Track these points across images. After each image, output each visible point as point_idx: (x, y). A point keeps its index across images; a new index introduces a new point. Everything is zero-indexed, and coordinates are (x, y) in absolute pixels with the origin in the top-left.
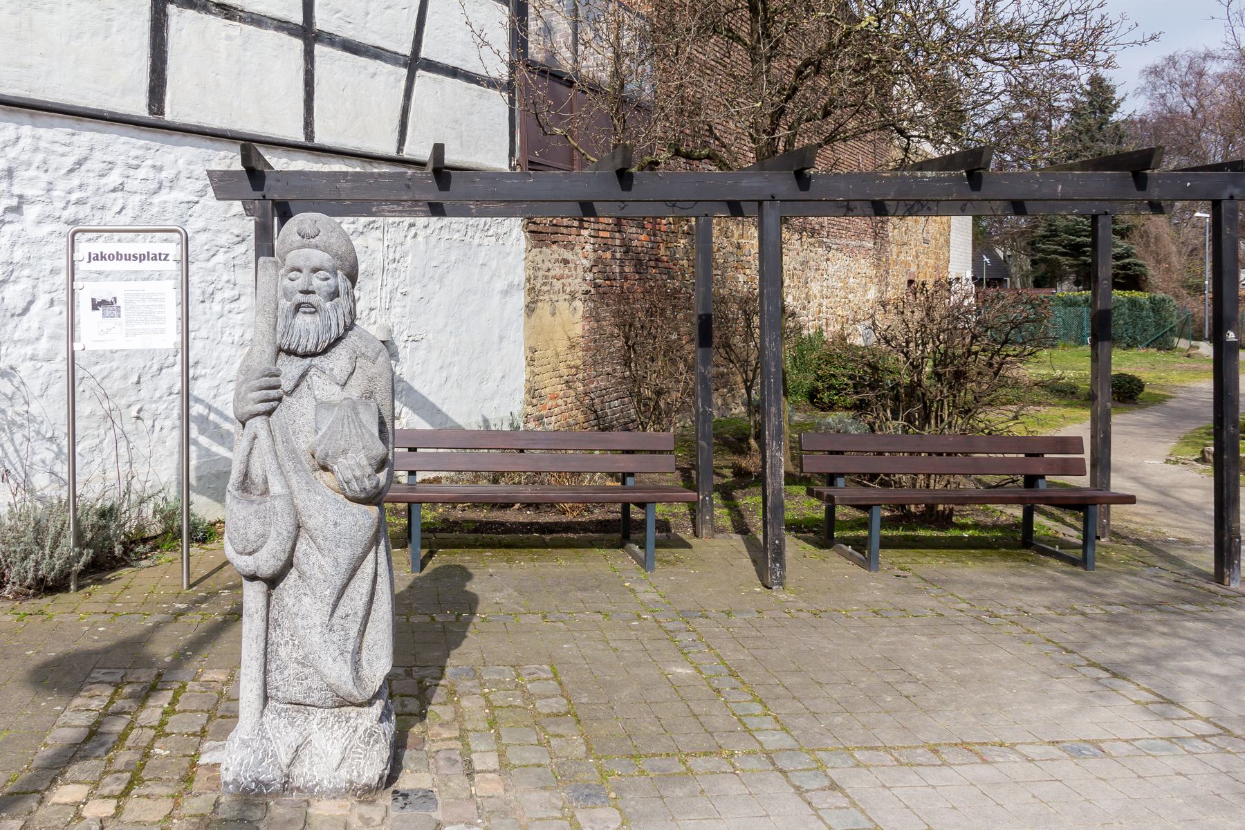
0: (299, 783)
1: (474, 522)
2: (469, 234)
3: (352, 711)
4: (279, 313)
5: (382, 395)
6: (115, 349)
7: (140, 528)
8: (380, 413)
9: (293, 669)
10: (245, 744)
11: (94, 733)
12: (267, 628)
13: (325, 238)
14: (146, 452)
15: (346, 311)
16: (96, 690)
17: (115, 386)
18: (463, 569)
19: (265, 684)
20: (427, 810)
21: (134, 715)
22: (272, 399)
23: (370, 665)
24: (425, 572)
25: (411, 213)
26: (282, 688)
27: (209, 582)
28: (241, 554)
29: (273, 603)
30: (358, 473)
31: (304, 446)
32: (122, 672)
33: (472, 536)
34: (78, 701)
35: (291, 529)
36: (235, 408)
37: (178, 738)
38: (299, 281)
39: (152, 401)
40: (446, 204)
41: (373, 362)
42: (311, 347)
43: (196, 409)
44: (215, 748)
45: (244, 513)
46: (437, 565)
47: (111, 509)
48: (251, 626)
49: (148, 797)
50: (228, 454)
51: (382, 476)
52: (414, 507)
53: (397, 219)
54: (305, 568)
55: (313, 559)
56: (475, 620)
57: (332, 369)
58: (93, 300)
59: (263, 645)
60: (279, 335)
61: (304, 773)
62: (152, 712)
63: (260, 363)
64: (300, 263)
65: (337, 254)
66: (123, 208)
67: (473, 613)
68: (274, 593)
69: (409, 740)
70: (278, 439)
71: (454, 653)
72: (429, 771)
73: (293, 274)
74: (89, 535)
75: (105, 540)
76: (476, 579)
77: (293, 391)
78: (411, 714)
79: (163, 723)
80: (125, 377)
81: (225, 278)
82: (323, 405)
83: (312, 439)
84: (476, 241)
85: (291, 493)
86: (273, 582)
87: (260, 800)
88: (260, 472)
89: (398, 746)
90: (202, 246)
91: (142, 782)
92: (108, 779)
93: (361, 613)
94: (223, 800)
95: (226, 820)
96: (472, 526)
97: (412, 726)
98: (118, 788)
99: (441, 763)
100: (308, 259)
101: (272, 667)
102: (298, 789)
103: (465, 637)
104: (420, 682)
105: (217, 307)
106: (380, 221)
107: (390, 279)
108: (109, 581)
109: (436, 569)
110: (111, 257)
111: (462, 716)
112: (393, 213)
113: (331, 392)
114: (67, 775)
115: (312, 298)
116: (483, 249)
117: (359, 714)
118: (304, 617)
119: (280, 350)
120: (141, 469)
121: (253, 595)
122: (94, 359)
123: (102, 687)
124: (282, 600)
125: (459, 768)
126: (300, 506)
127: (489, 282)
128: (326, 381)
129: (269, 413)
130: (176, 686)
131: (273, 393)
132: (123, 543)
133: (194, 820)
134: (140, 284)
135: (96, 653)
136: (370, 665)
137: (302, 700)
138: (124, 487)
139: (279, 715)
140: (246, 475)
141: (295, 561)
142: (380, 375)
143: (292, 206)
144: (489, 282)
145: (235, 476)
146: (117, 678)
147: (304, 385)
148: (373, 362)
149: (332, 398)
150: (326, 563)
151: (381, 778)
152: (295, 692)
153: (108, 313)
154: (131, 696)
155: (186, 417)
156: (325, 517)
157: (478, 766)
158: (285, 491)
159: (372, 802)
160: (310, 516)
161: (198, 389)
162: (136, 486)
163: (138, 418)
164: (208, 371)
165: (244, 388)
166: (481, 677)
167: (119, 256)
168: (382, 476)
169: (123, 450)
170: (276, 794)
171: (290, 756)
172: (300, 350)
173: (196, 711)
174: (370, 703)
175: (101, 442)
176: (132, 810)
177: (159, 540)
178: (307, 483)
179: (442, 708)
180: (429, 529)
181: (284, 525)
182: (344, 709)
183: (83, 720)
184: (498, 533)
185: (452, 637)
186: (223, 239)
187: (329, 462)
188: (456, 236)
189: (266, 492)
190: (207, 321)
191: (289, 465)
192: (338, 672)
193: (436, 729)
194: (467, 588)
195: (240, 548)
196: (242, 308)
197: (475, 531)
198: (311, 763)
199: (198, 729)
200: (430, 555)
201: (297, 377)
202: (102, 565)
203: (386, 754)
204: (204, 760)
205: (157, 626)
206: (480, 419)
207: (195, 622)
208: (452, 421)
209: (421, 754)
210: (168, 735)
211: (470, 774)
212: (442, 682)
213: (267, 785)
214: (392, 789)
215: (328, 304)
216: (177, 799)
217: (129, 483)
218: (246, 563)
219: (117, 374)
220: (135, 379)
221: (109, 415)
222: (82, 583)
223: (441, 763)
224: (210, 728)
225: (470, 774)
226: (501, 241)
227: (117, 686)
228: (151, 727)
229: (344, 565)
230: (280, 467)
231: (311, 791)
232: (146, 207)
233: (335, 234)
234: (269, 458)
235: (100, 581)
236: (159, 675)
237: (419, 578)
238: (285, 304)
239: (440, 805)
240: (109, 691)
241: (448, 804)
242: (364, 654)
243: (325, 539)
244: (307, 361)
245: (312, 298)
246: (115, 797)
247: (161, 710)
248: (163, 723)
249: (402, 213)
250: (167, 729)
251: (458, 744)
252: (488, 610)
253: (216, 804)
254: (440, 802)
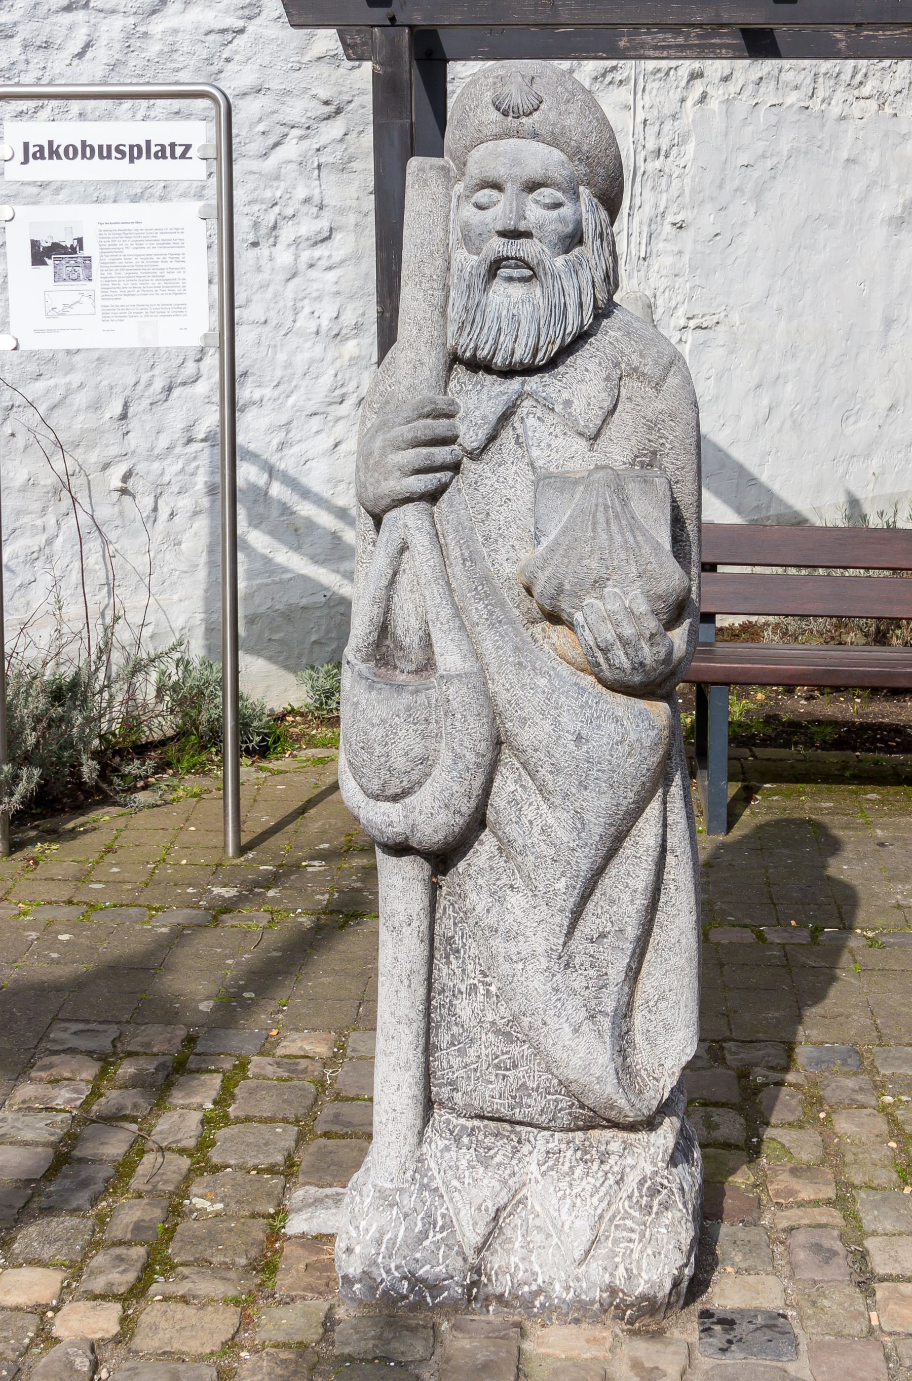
0: (503, 1285)
1: (835, 723)
2: (821, 94)
3: (614, 1140)
4: (453, 280)
5: (675, 461)
6: (73, 346)
7: (131, 723)
8: (674, 500)
9: (486, 1045)
10: (386, 1199)
11: (64, 1158)
12: (431, 957)
13: (552, 116)
14: (141, 562)
15: (599, 276)
16: (64, 1067)
17: (77, 425)
18: (820, 829)
19: (427, 1074)
20: (778, 1356)
21: (145, 1123)
22: (440, 468)
23: (652, 1044)
24: (737, 832)
25: (705, 51)
26: (463, 1084)
27: (279, 841)
28: (377, 798)
29: (443, 903)
30: (628, 631)
31: (508, 569)
32: (113, 1031)
33: (833, 757)
34: (27, 1091)
35: (482, 747)
36: (361, 487)
37: (239, 1176)
38: (499, 209)
39: (152, 456)
40: (782, 33)
41: (657, 387)
42: (522, 354)
43: (247, 473)
44: (318, 1202)
45: (383, 711)
46: (762, 819)
47: (75, 684)
48: (397, 945)
49: (184, 1300)
50: (346, 590)
51: (679, 637)
52: (714, 695)
53: (664, 64)
54: (512, 831)
55: (529, 813)
56: (853, 943)
57: (568, 403)
58: (35, 244)
59: (422, 991)
60: (452, 328)
61: (510, 1267)
62: (182, 1119)
63: (412, 388)
64: (498, 171)
65: (578, 150)
66: (88, 45)
67: (847, 927)
68: (445, 881)
69: (728, 1203)
70: (454, 552)
71: (812, 1013)
72: (775, 1272)
73: (484, 196)
74: (31, 739)
75: (62, 748)
76: (848, 852)
77: (484, 449)
78: (727, 1145)
79: (204, 1144)
80: (96, 406)
81: (301, 193)
82: (550, 486)
83: (526, 555)
84: (836, 109)
85: (483, 670)
86: (443, 859)
87: (419, 1318)
88: (414, 623)
89: (708, 1212)
90: (252, 125)
91: (169, 1267)
92: (100, 1259)
93: (632, 932)
94: (341, 1313)
95: (350, 1358)
96: (830, 734)
97: (733, 1171)
98: (122, 1279)
99: (802, 1255)
100: (516, 162)
101: (443, 1038)
102: (500, 1298)
103: (833, 979)
104: (743, 1075)
105: (284, 257)
106: (628, 67)
107: (648, 194)
108: (73, 834)
109: (760, 828)
110: (71, 152)
111: (839, 1154)
112: (663, 51)
113: (564, 452)
114: (17, 1247)
115: (526, 249)
116: (851, 127)
117: (627, 1146)
118: (510, 936)
119: (454, 359)
120: (132, 601)
121: (400, 886)
122: (32, 368)
123: (75, 1061)
124: (463, 897)
125: (839, 1269)
126: (502, 698)
127: (862, 200)
128: (556, 426)
129: (433, 496)
130: (227, 1064)
131: (442, 454)
132: (96, 755)
133: (284, 1355)
134: (124, 211)
135: (58, 988)
136: (652, 1044)
137: (505, 1112)
138: (97, 637)
139: (457, 1140)
140: (384, 629)
141: (491, 815)
142: (672, 417)
143: (447, 41)
144: (862, 200)
145: (361, 628)
146: (104, 1043)
147: (507, 435)
148: (657, 387)
149: (570, 466)
150: (558, 822)
151: (676, 1284)
152: (491, 1093)
153: (64, 271)
154: (137, 1082)
155: (229, 495)
156: (557, 723)
157: (880, 1264)
158: (469, 666)
159: (657, 1335)
160: (523, 721)
161: (253, 430)
162: (123, 634)
163: (124, 491)
164: (267, 392)
165: (378, 443)
166: (873, 1070)
167: (86, 151)
168: (679, 637)
169: (94, 560)
170: (453, 1308)
171: (482, 1229)
172: (498, 360)
173: (271, 1120)
174: (650, 1124)
175: (49, 542)
176: (154, 1328)
177: (172, 750)
178: (517, 649)
179: (794, 1134)
180: (741, 737)
181: (467, 738)
182: (595, 1133)
183: (40, 1130)
184: (890, 750)
185: (804, 978)
186: (297, 110)
187: (565, 605)
188: (792, 98)
189: (427, 666)
190: (264, 287)
191: (477, 610)
192: (585, 1057)
193: (783, 1181)
194: (832, 871)
195: (375, 786)
196: (337, 257)
197: (840, 744)
198: (526, 1246)
199: (280, 1158)
200: (746, 796)
201: (493, 418)
202: (56, 800)
203: (687, 1234)
204: (296, 1225)
205: (179, 935)
206: (842, 499)
207: (257, 929)
208: (781, 501)
209: (755, 1234)
210: (216, 1169)
211: (866, 1282)
212: (791, 1077)
213: (435, 1287)
214: (697, 1307)
215: (560, 261)
216: (245, 1306)
217: (108, 631)
218: (384, 818)
219: (81, 399)
220: (118, 410)
221: (65, 485)
222: (18, 837)
223: (802, 1255)
224: (304, 1158)
225: (866, 1282)
226: (888, 110)
227: (106, 1060)
228: (182, 1151)
229: (597, 829)
230: (458, 612)
231: (527, 1304)
232: (135, 43)
233: (575, 108)
234: (434, 594)
235: (54, 835)
236: (191, 1040)
237: (723, 846)
238: (468, 261)
239: (803, 1347)
240: (89, 1071)
241: (821, 1346)
242: (639, 1018)
243: (556, 770)
244: (515, 384)
245: (526, 249)
246: (117, 1298)
247: (197, 1116)
248: (204, 1144)
249: (682, 52)
250: (215, 1156)
251: (835, 1216)
252: (880, 921)
253: (329, 1323)
254: (803, 1340)
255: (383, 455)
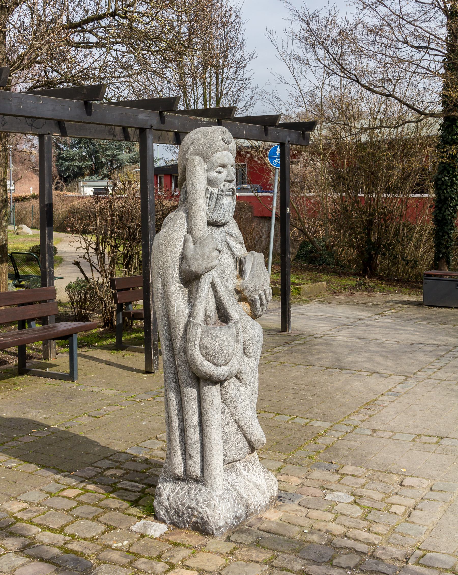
156: (254, 331)
255: (210, 253)
